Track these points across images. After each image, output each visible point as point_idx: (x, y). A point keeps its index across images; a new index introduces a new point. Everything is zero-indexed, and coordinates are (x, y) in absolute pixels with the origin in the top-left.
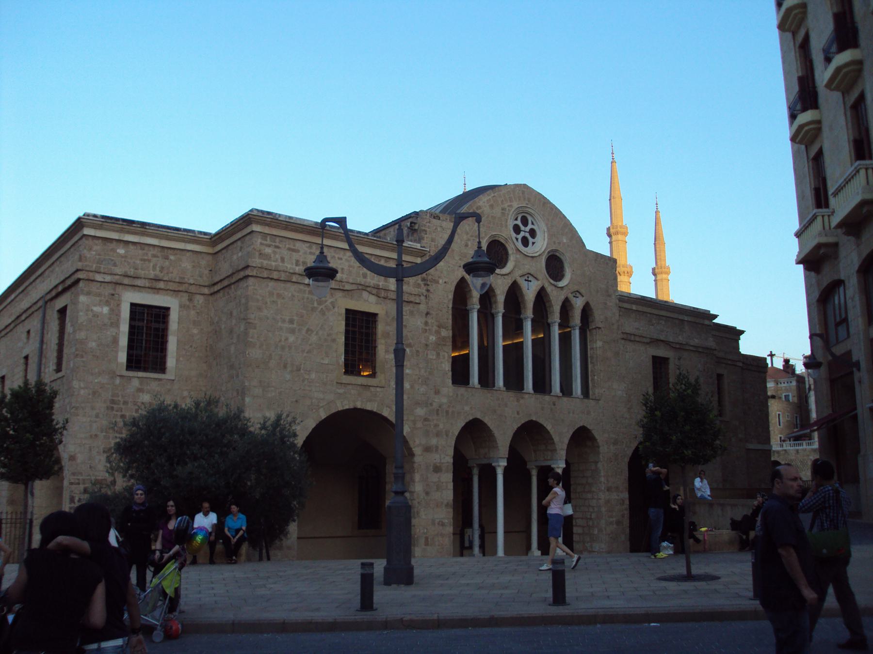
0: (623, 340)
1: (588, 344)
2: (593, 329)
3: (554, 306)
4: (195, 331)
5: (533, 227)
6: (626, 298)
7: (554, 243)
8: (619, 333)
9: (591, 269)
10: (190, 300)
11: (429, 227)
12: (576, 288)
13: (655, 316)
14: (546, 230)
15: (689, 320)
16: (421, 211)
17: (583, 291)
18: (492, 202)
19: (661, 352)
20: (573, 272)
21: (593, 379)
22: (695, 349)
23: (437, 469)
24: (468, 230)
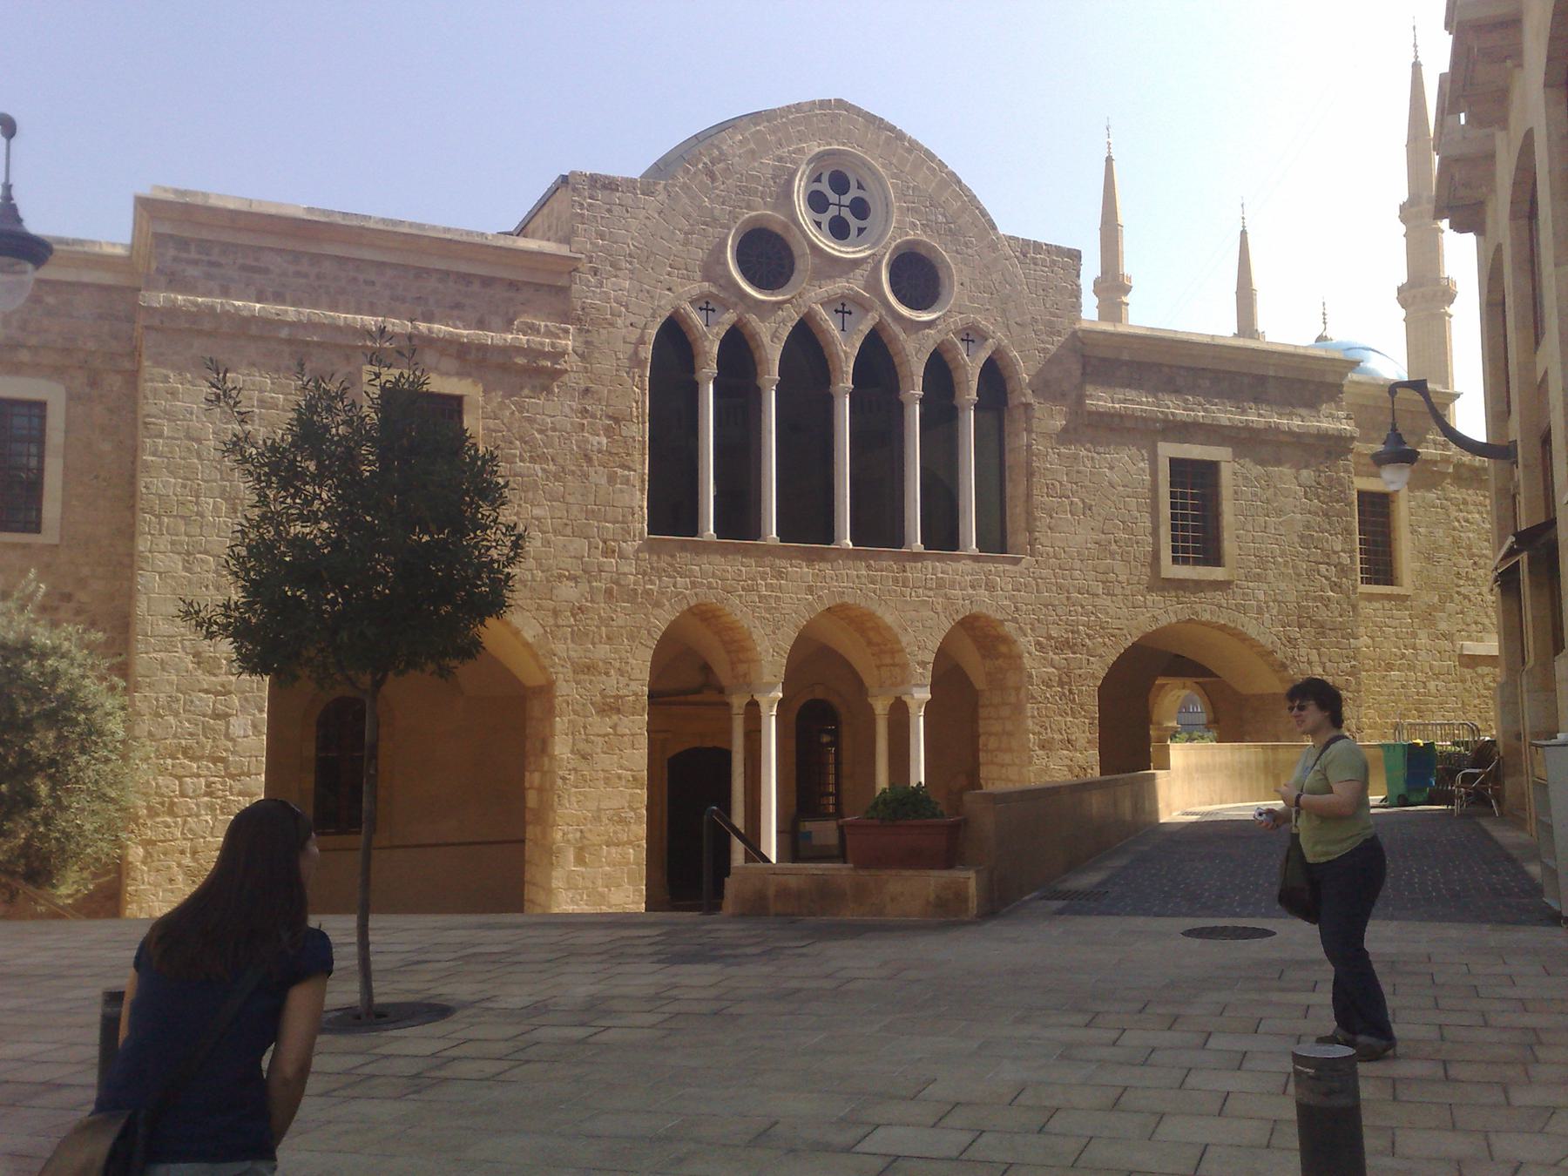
4: (106, 447)
5: (860, 193)
10: (93, 383)
16: (573, 173)
23: (610, 707)
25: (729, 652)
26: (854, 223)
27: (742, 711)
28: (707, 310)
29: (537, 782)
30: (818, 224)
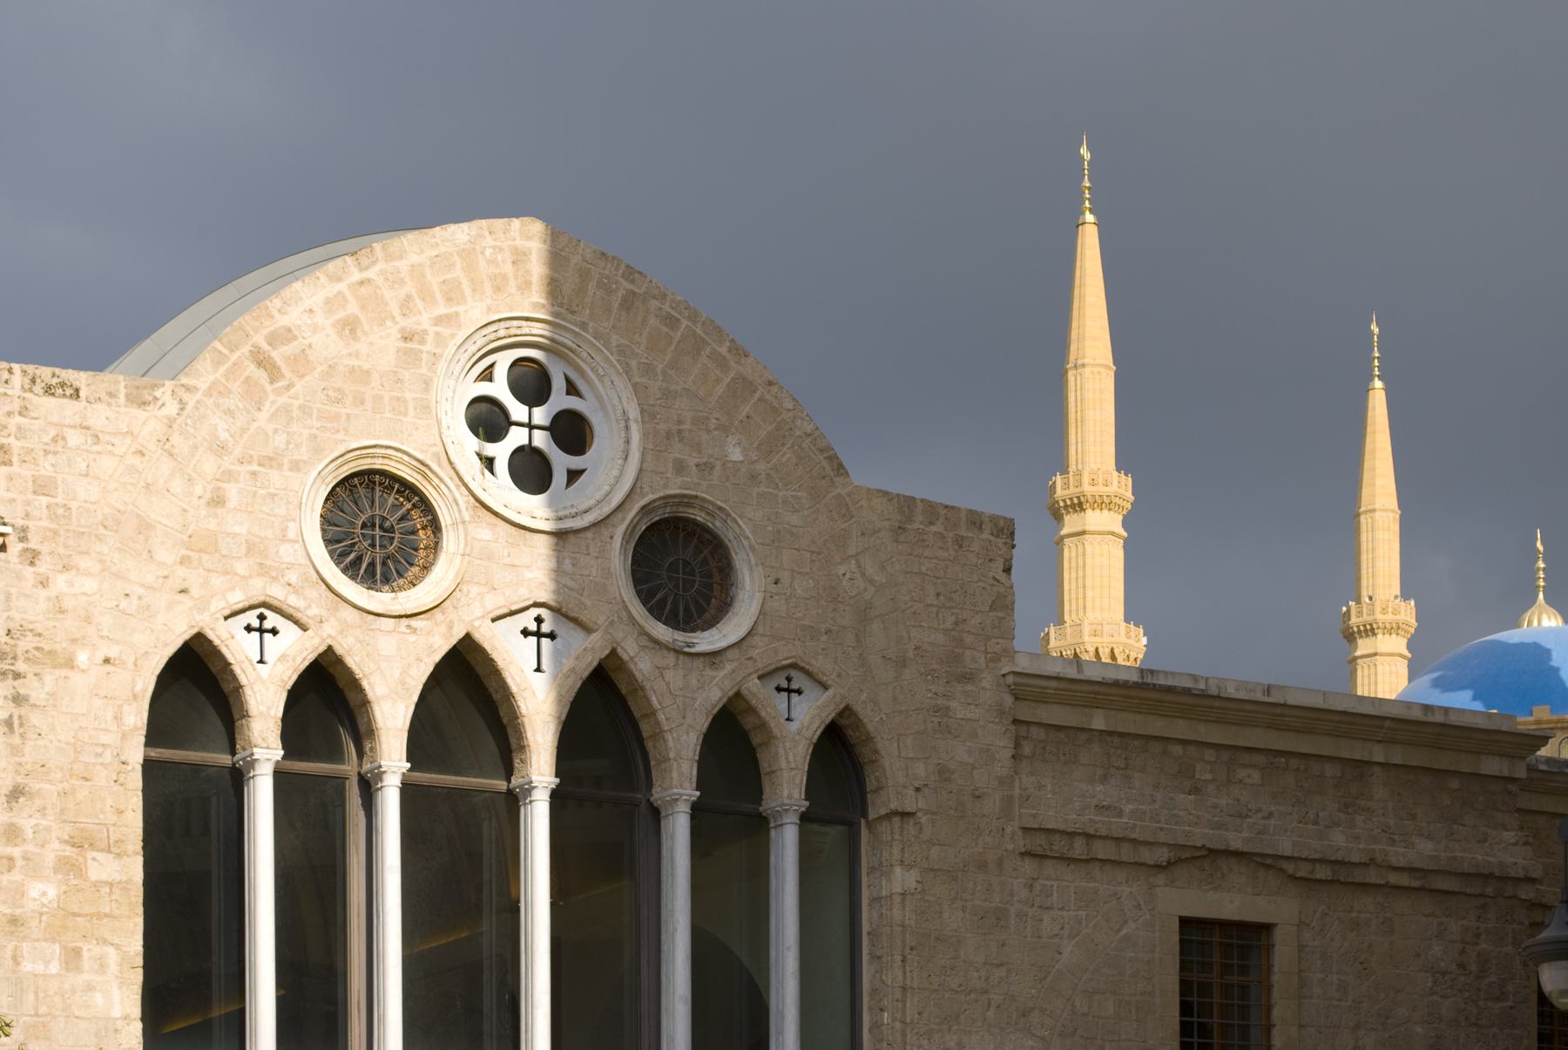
0: (1027, 861)
1: (864, 880)
2: (881, 818)
3: (669, 737)
5: (573, 403)
6: (1054, 684)
7: (680, 467)
8: (1009, 830)
9: (870, 570)
11: (21, 433)
12: (785, 654)
13: (1209, 755)
14: (634, 412)
15: (1398, 760)
17: (821, 664)
18: (352, 308)
20: (773, 588)
21: (876, 1026)
22: (1416, 884)
24: (223, 435)
26: (561, 461)
28: (261, 631)
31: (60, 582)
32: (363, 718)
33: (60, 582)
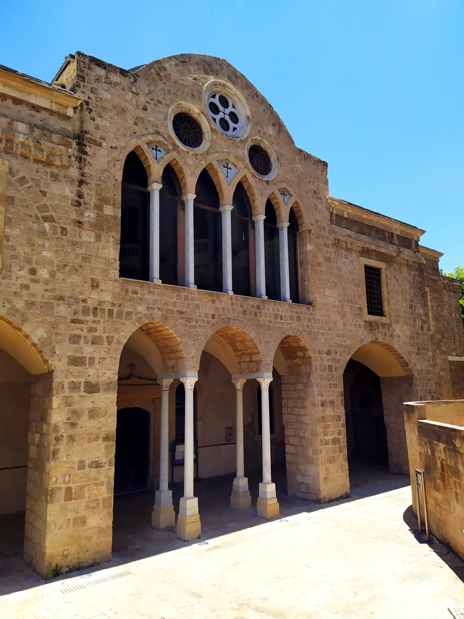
19: (373, 263)
25: (162, 354)
27: (168, 389)
29: (37, 441)
30: (215, 120)
31: (98, 120)
32: (183, 182)
33: (98, 120)
